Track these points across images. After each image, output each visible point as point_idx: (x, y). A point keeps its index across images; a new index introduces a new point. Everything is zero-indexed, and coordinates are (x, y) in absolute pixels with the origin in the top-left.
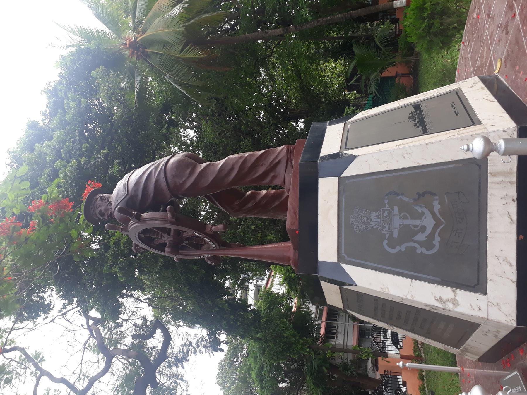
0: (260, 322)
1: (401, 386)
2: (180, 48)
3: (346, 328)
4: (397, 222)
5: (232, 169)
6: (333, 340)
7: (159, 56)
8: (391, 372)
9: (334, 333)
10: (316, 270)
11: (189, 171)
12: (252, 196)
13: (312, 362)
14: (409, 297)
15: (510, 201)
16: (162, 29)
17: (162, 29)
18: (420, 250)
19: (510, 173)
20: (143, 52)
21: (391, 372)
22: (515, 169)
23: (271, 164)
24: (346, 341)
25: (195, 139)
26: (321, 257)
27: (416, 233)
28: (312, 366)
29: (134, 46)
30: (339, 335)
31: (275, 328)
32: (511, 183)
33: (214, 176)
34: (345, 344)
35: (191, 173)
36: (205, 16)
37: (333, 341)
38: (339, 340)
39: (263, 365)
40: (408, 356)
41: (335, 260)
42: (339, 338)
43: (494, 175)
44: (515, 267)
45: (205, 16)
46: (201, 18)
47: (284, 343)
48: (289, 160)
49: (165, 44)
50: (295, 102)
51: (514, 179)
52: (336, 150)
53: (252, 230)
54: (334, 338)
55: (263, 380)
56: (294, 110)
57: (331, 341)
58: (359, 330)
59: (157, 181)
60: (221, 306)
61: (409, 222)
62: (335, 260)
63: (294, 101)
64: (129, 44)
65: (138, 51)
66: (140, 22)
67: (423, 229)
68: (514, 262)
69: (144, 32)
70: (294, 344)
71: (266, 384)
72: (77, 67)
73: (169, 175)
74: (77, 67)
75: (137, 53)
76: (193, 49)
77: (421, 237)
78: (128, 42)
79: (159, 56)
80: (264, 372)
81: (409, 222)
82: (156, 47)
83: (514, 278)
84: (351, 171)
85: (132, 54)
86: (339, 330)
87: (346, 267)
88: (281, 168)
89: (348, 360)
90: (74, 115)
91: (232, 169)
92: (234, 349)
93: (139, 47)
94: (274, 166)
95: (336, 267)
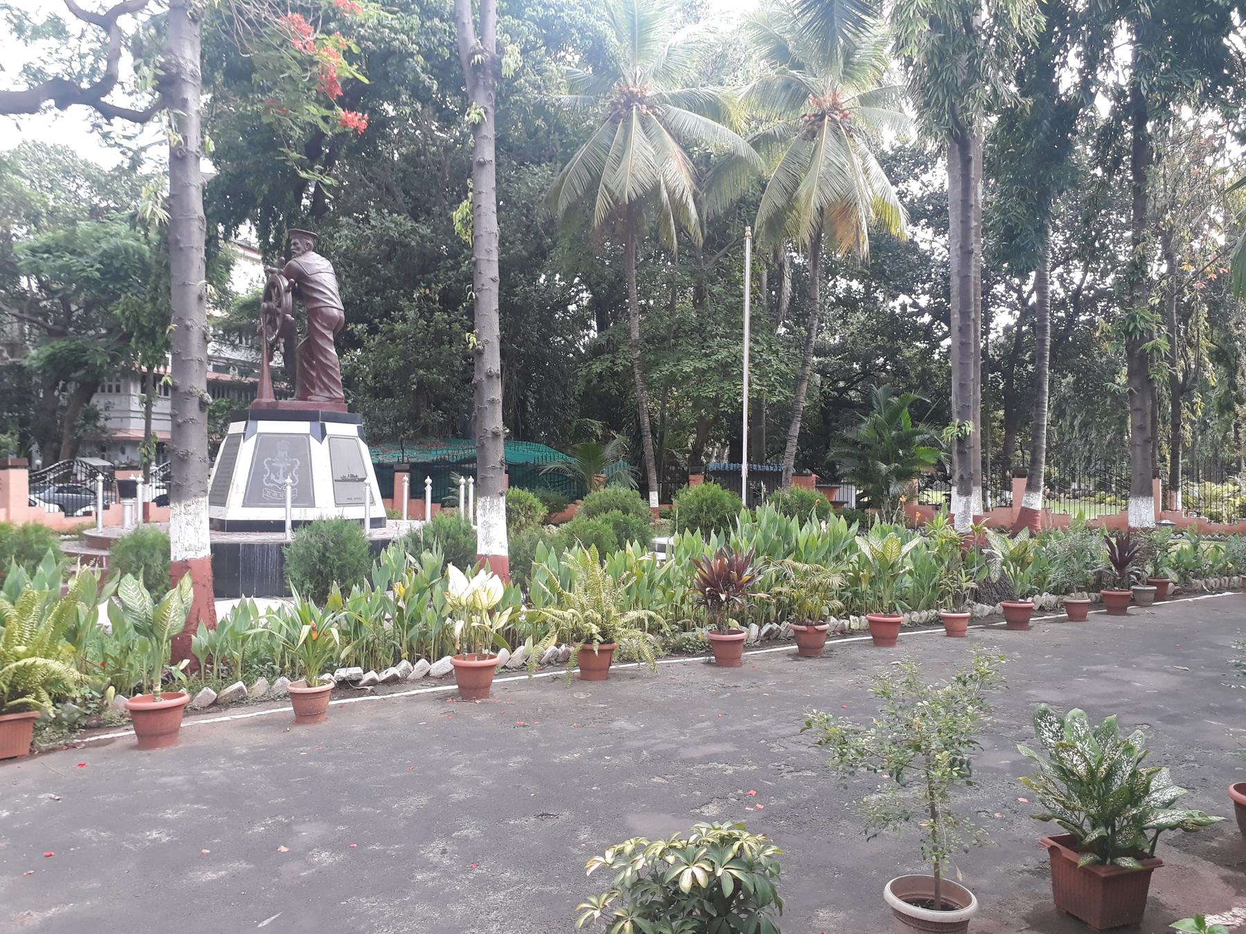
1: (83, 510)
4: (282, 466)
5: (327, 359)
10: (251, 419)
18: (265, 477)
26: (260, 423)
27: (275, 474)
34: (132, 415)
35: (323, 327)
39: (81, 255)
41: (259, 431)
47: (154, 328)
48: (331, 399)
52: (328, 432)
55: (50, 253)
61: (281, 472)
62: (259, 431)
67: (278, 478)
69: (644, 121)
70: (154, 343)
71: (42, 258)
76: (609, 203)
77: (273, 477)
80: (67, 257)
81: (281, 472)
84: (313, 442)
87: (254, 437)
88: (327, 394)
89: (106, 419)
91: (327, 359)
94: (328, 388)
95: (254, 432)
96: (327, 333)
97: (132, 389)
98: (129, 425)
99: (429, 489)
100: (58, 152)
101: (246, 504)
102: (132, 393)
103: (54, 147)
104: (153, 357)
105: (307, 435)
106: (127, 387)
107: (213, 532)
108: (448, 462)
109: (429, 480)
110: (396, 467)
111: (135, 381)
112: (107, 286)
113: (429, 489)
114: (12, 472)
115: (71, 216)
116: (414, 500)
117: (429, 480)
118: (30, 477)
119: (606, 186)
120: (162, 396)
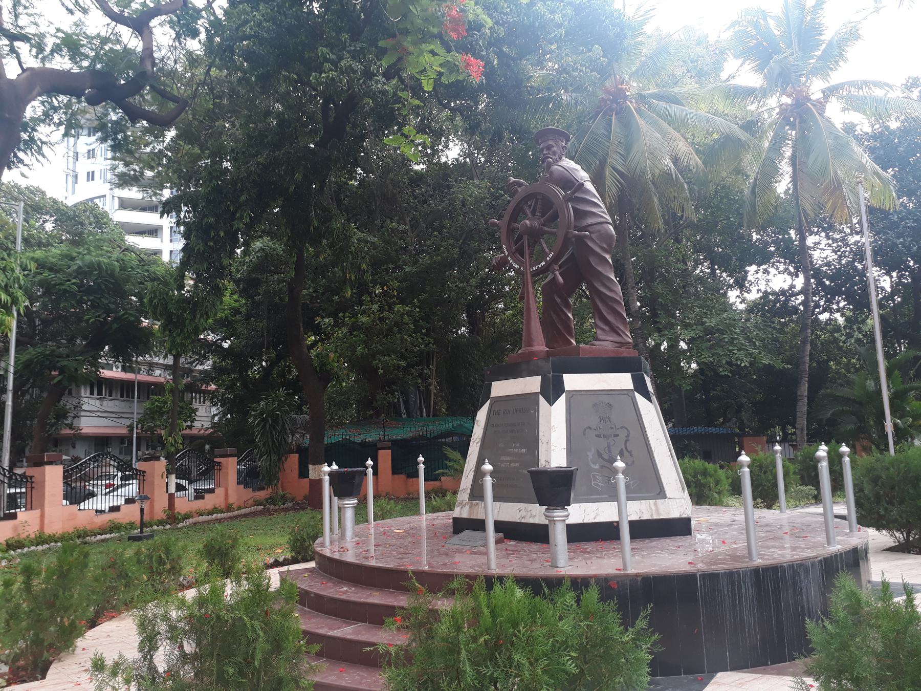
0: (216, 278)
2: (620, 168)
3: (119, 415)
6: (88, 391)
7: (606, 133)
8: (144, 480)
9: (100, 393)
11: (605, 246)
12: (568, 306)
13: (68, 356)
14: (552, 448)
15: (639, 515)
16: (648, 144)
17: (648, 144)
19: (658, 514)
20: (612, 110)
21: (144, 480)
22: (661, 517)
23: (618, 327)
24: (88, 414)
25: (443, 159)
28: (63, 357)
29: (619, 95)
30: (98, 403)
31: (208, 301)
32: (652, 515)
33: (603, 272)
34: (83, 414)
36: (656, 200)
37: (85, 393)
38: (89, 402)
39: (57, 272)
40: (174, 505)
42: (92, 402)
43: (655, 504)
44: (594, 521)
45: (656, 200)
46: (653, 194)
49: (628, 148)
50: (495, 323)
51: (655, 517)
53: (360, 265)
54: (92, 393)
56: (484, 320)
57: (85, 388)
58: (108, 437)
59: (594, 214)
60: (238, 215)
63: (498, 321)
64: (621, 89)
65: (612, 101)
66: (650, 107)
68: (597, 520)
70: (182, 330)
72: (604, 21)
73: (597, 227)
74: (604, 21)
75: (609, 99)
78: (624, 87)
79: (606, 133)
82: (618, 131)
83: (585, 521)
85: (608, 92)
86: (105, 403)
88: (613, 337)
89: (74, 418)
90: (542, 16)
91: (611, 290)
92: (75, 216)
93: (617, 104)
94: (614, 330)
96: (608, 257)
97: (83, 391)
98: (80, 423)
99: (422, 467)
100: (32, 192)
101: (661, 493)
102: (83, 394)
103: (27, 188)
104: (182, 345)
105: (536, 394)
106: (79, 392)
107: (574, 546)
108: (427, 438)
109: (421, 458)
110: (379, 445)
111: (85, 385)
112: (81, 297)
113: (422, 467)
114: (48, 468)
115: (44, 241)
116: (396, 476)
117: (421, 458)
118: (64, 472)
119: (614, 168)
120: (107, 397)
